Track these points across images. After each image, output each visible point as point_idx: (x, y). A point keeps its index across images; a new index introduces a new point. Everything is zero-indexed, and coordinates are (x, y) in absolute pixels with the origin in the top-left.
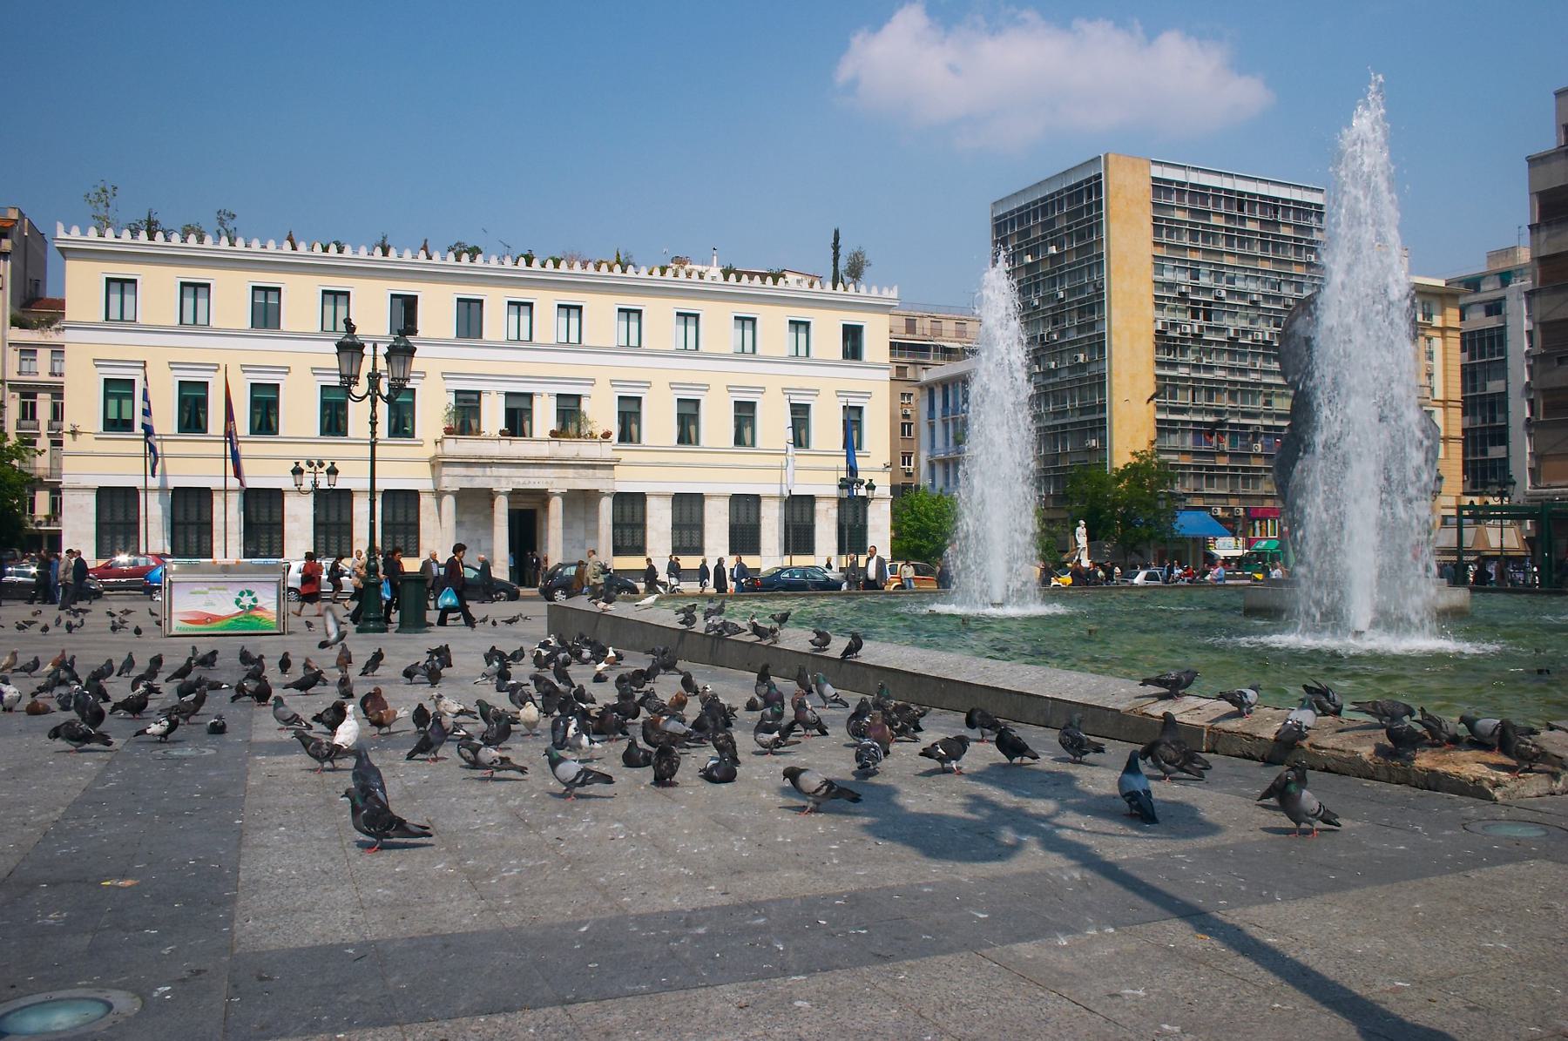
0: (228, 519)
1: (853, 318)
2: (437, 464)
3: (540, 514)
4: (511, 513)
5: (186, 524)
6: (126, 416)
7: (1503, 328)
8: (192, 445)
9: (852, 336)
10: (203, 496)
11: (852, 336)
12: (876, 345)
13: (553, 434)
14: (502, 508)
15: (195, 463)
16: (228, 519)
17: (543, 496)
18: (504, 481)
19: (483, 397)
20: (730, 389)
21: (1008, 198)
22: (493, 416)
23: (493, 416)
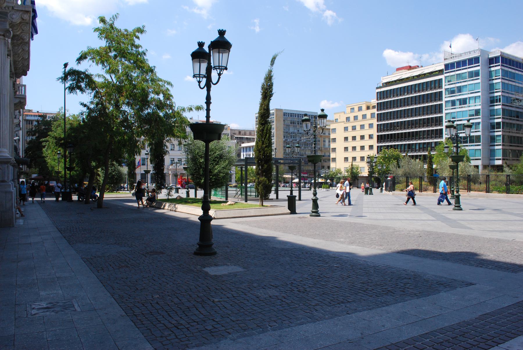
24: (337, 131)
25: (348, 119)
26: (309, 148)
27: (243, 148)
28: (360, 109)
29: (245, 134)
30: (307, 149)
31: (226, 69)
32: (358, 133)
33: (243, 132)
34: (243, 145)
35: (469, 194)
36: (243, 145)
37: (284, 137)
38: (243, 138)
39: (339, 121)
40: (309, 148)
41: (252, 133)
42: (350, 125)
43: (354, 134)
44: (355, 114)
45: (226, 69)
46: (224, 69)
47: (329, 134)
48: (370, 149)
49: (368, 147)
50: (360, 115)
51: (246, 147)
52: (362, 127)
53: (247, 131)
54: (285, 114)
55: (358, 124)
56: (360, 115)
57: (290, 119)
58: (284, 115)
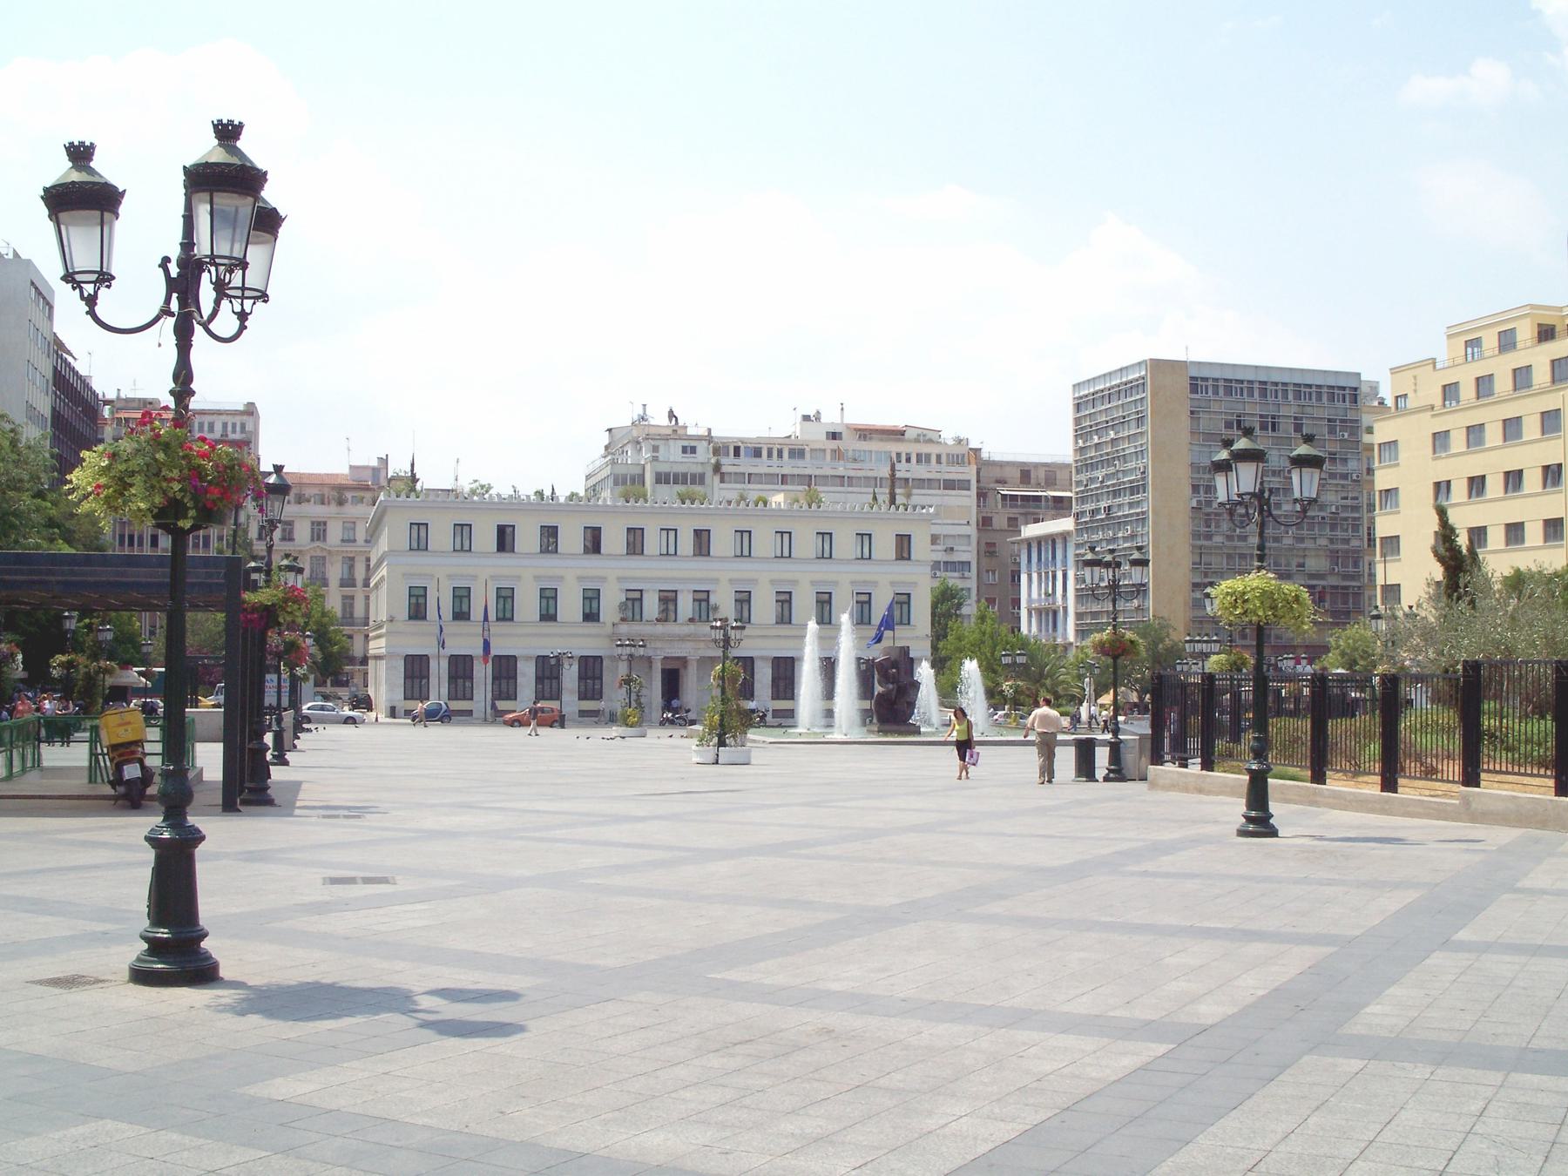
0: (482, 673)
1: (635, 523)
2: (614, 637)
3: (682, 671)
4: (663, 671)
5: (594, 678)
6: (552, 611)
7: (494, 698)
8: (461, 626)
9: (904, 542)
10: (468, 660)
11: (904, 542)
12: (921, 548)
13: (691, 620)
14: (658, 667)
15: (465, 641)
16: (482, 673)
17: (684, 661)
18: (660, 652)
19: (645, 595)
20: (813, 583)
21: (348, 808)
22: (651, 606)
23: (651, 606)
24: (1403, 455)
25: (1450, 391)
26: (1323, 542)
27: (1028, 542)
28: (1507, 342)
29: (1051, 482)
30: (1308, 544)
31: (263, 296)
32: (1494, 461)
33: (1042, 474)
34: (1030, 531)
35: (1466, 801)
36: (1030, 531)
37: (1195, 488)
38: (1038, 498)
39: (1412, 403)
40: (1323, 542)
41: (1061, 476)
42: (1456, 423)
43: (1475, 464)
44: (1480, 369)
45: (263, 296)
46: (256, 298)
47: (1370, 471)
48: (1547, 538)
49: (1540, 526)
50: (1501, 368)
51: (1040, 541)
52: (1512, 428)
53: (1037, 465)
54: (1196, 384)
55: (1491, 417)
56: (1501, 368)
57: (1221, 408)
58: (1194, 388)
